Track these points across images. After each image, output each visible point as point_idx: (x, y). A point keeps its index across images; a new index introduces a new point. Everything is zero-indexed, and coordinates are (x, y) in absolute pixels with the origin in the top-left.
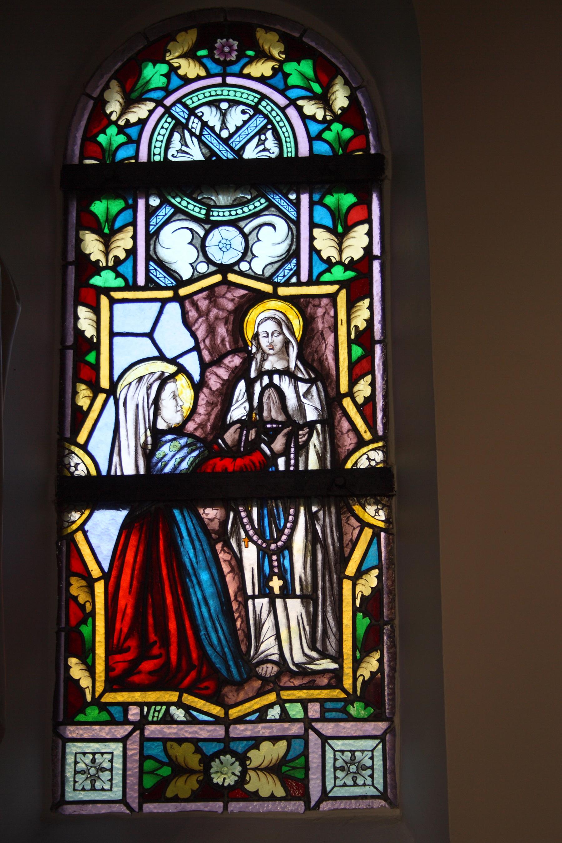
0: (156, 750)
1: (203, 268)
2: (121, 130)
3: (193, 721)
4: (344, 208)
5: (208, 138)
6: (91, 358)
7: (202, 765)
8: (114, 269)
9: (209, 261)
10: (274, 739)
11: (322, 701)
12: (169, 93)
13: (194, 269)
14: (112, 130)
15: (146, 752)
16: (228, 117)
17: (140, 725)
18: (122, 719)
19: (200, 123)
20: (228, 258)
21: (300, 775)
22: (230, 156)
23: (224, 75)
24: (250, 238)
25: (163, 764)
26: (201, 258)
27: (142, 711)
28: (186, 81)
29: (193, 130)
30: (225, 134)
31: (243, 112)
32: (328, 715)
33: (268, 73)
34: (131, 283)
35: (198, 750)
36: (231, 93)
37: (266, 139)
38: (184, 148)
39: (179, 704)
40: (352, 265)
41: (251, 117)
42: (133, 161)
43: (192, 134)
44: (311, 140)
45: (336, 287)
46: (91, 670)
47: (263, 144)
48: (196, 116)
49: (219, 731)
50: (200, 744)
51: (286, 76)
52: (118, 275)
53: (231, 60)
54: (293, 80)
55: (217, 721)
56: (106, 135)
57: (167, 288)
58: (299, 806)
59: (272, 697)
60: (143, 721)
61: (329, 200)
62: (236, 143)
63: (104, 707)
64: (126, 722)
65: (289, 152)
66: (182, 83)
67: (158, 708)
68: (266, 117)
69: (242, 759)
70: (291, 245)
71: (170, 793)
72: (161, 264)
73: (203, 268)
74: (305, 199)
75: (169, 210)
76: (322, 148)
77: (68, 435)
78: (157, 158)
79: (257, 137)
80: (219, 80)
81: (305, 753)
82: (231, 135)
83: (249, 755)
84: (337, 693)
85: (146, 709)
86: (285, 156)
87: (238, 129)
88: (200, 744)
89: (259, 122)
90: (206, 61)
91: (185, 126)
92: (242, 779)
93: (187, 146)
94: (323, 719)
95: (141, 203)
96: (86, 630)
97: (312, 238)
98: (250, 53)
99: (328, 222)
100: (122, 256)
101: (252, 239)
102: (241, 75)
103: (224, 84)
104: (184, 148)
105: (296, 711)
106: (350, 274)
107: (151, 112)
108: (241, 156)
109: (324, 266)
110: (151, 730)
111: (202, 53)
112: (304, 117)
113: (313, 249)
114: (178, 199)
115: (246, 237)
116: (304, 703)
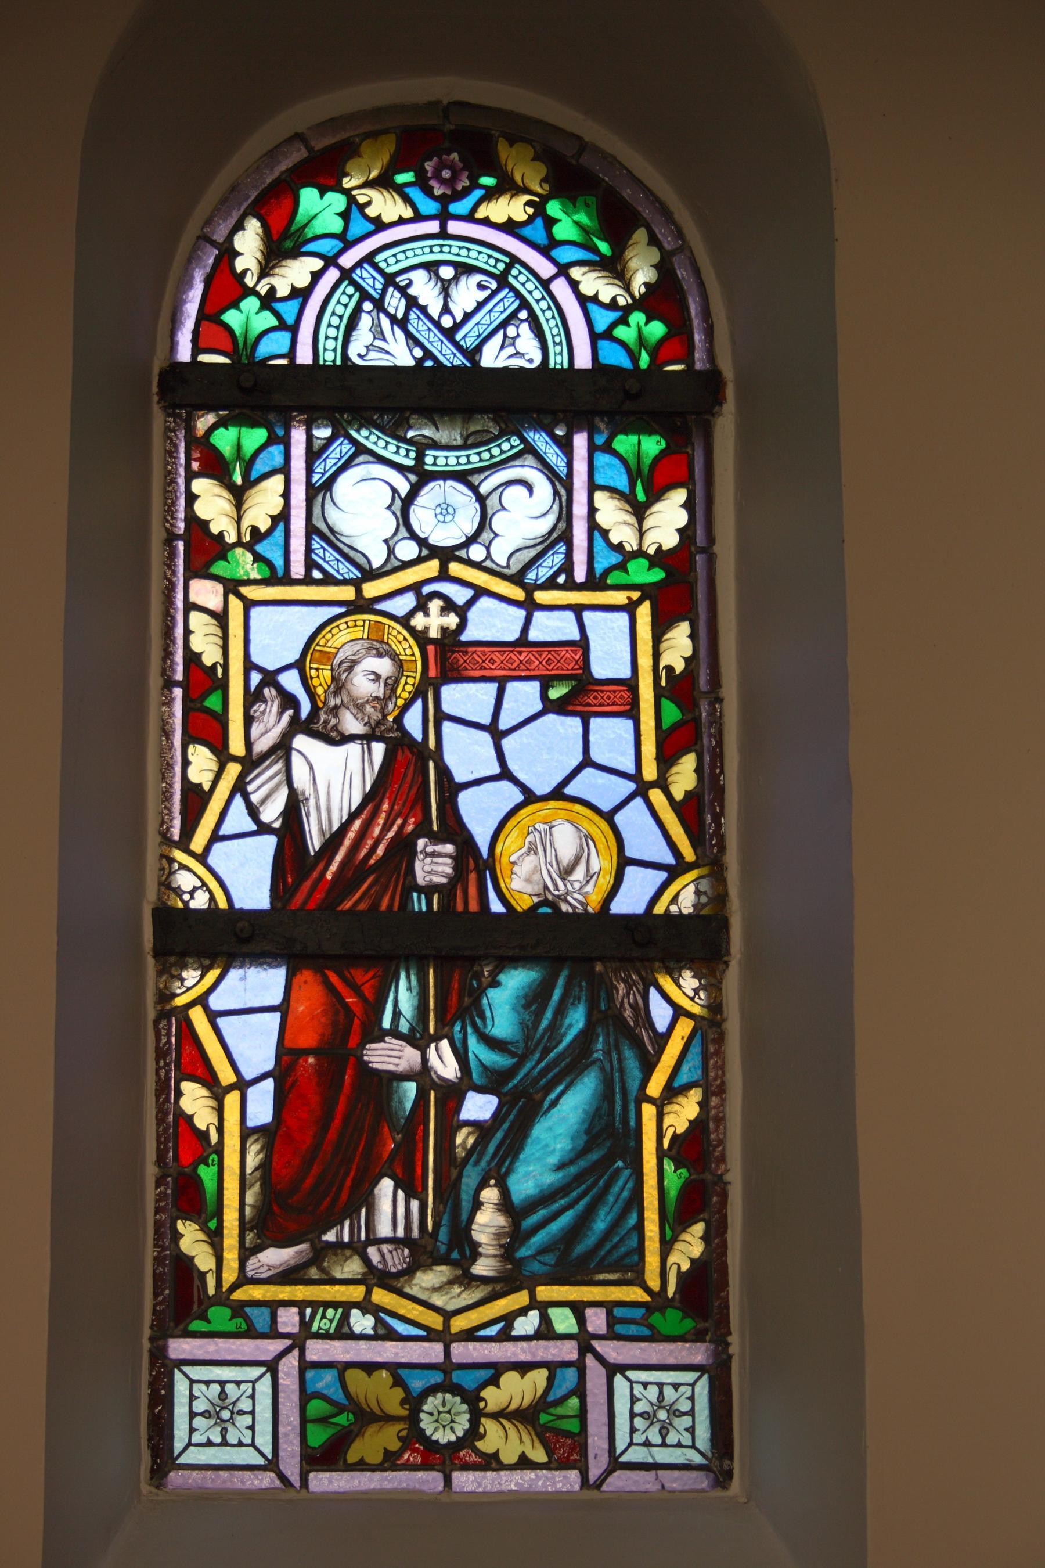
0: (325, 1381)
1: (408, 550)
2: (268, 301)
3: (384, 1333)
4: (647, 461)
5: (418, 325)
6: (213, 702)
7: (407, 1407)
8: (249, 547)
9: (422, 542)
10: (523, 1368)
11: (609, 1306)
12: (348, 245)
13: (391, 552)
14: (251, 303)
15: (310, 1389)
16: (454, 292)
17: (298, 1342)
18: (266, 1329)
19: (403, 302)
20: (444, 536)
21: (573, 1426)
22: (459, 360)
23: (444, 217)
24: (489, 502)
25: (340, 1409)
26: (403, 532)
27: (302, 1315)
28: (379, 225)
29: (392, 311)
30: (447, 322)
31: (481, 287)
32: (619, 1329)
33: (520, 216)
34: (280, 572)
35: (398, 1382)
36: (453, 251)
37: (518, 335)
38: (378, 343)
39: (366, 1306)
40: (660, 558)
41: (494, 293)
42: (284, 362)
43: (393, 319)
44: (595, 337)
45: (635, 595)
46: (215, 1239)
47: (513, 344)
48: (397, 287)
49: (434, 1352)
50: (400, 1371)
51: (550, 222)
52: (258, 558)
53: (433, 188)
54: (564, 230)
55: (431, 1335)
56: (241, 312)
57: (345, 582)
58: (568, 1481)
59: (522, 1298)
60: (305, 1332)
61: (624, 443)
62: (468, 336)
63: (239, 1309)
64: (274, 1334)
65: (558, 360)
66: (371, 227)
67: (330, 1312)
68: (518, 295)
69: (472, 1399)
70: (559, 519)
71: (352, 1457)
72: (331, 538)
73: (408, 550)
74: (580, 441)
75: (347, 448)
76: (613, 356)
77: (176, 833)
78: (329, 356)
79: (501, 333)
80: (433, 227)
81: (580, 1391)
82: (457, 326)
83: (483, 1394)
84: (636, 1294)
85: (308, 1311)
86: (552, 365)
87: (468, 317)
88: (400, 1371)
89: (508, 303)
90: (415, 194)
91: (379, 305)
92: (474, 1433)
93: (384, 339)
94: (612, 1335)
95: (298, 436)
96: (207, 1174)
97: (592, 510)
98: (488, 181)
99: (622, 482)
100: (264, 525)
101: (492, 502)
102: (470, 218)
103: (443, 234)
104: (378, 343)
105: (564, 1321)
106: (657, 575)
107: (317, 276)
108: (476, 364)
109: (615, 558)
110: (316, 1350)
111: (404, 178)
112: (583, 301)
113: (593, 526)
114: (365, 432)
115: (481, 500)
116: (578, 1309)
